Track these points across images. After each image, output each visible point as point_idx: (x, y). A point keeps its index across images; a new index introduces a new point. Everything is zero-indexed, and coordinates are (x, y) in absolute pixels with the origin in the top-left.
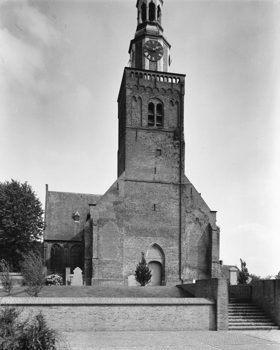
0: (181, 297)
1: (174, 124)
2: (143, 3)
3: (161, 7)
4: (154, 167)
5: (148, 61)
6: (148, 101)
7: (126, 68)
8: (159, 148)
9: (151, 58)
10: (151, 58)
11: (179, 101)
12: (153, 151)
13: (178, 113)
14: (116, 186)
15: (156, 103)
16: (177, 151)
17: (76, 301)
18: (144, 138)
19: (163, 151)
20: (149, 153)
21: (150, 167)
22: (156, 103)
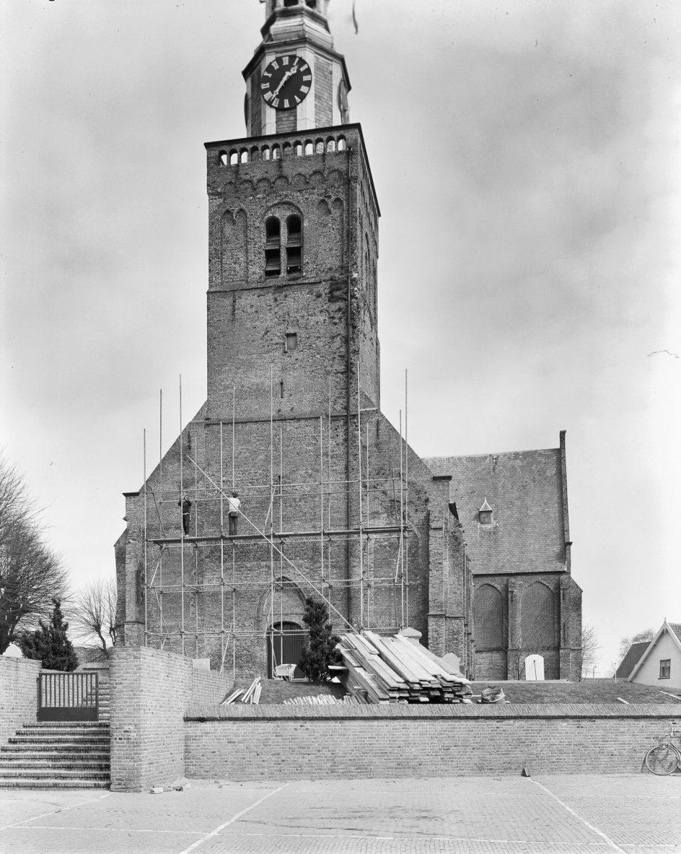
1: (332, 261)
4: (278, 380)
5: (273, 112)
8: (291, 330)
10: (281, 103)
11: (342, 197)
15: (282, 215)
16: (340, 329)
18: (254, 310)
19: (302, 334)
20: (266, 348)
22: (282, 215)
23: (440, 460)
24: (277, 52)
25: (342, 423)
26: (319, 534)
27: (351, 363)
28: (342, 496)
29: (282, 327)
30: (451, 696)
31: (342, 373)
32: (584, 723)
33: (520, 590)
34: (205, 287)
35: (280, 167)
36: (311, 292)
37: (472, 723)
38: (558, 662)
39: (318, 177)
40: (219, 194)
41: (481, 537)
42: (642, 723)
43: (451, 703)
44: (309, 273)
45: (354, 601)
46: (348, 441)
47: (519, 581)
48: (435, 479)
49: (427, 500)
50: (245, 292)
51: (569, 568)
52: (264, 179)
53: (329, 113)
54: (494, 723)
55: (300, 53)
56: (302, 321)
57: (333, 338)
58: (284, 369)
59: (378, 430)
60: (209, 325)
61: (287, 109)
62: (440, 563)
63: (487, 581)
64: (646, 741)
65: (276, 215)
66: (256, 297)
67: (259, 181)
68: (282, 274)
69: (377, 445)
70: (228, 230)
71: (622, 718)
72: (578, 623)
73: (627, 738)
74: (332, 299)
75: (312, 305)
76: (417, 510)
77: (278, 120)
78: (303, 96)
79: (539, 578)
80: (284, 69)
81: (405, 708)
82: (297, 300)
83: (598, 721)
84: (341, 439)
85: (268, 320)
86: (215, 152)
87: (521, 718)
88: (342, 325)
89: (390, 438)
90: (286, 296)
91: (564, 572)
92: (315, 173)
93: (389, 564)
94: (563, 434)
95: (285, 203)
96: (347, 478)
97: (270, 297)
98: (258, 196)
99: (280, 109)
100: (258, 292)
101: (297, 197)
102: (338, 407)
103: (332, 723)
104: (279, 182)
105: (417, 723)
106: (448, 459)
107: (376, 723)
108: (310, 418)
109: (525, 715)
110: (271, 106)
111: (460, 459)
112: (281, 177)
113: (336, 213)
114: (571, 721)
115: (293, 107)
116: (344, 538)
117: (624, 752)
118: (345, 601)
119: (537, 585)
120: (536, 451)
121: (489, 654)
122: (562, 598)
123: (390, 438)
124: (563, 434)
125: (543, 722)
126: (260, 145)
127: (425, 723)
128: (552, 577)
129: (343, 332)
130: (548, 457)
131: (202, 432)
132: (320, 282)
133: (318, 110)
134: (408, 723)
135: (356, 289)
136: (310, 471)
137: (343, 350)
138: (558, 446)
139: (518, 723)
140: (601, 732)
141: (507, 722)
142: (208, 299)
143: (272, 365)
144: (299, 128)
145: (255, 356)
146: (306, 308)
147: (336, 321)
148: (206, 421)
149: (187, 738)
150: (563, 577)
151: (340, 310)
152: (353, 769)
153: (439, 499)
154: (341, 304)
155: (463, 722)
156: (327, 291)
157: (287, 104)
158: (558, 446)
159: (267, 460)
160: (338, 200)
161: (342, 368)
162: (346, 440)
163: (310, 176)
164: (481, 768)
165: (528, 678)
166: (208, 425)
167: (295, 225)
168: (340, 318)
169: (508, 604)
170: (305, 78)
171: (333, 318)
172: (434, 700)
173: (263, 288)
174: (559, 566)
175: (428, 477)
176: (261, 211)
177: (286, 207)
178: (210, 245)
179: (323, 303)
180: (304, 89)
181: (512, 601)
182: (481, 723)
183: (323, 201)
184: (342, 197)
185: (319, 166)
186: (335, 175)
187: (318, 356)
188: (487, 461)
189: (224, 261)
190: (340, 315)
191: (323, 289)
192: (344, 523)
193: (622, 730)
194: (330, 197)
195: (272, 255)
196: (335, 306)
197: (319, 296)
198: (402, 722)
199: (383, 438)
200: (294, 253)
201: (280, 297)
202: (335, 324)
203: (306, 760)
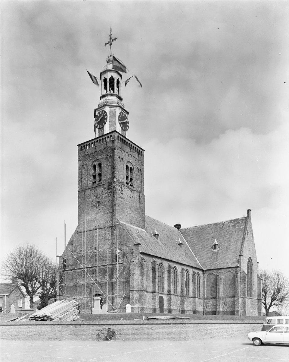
0: (212, 315)
1: (109, 176)
2: (105, 77)
3: (120, 80)
4: (95, 217)
5: (98, 129)
6: (92, 164)
7: (82, 147)
8: (98, 201)
9: (100, 126)
10: (100, 126)
11: (111, 155)
12: (95, 204)
13: (218, 292)
14: (72, 239)
15: (96, 163)
16: (111, 198)
17: (200, 321)
18: (89, 195)
19: (101, 201)
20: (92, 207)
21: (92, 218)
22: (96, 163)
23: (204, 226)
24: (99, 111)
25: (111, 229)
26: (97, 266)
27: (113, 209)
28: (111, 252)
29: (96, 200)
30: (46, 319)
31: (111, 212)
32: (77, 326)
33: (222, 275)
34: (78, 190)
35: (96, 148)
36: (103, 188)
37: (46, 326)
38: (235, 302)
39: (105, 150)
40: (81, 160)
41: (212, 255)
42: (95, 326)
43: (46, 321)
44: (103, 182)
45: (114, 286)
46: (112, 235)
47: (221, 272)
48: (135, 245)
49: (133, 252)
50: (87, 190)
51: (240, 265)
52: (92, 153)
53: (115, 125)
54: (52, 326)
55: (104, 110)
56: (101, 197)
57: (109, 201)
58: (97, 213)
59: (120, 230)
60: (78, 202)
61: (102, 128)
62: (133, 273)
63: (211, 272)
64: (96, 331)
65: (95, 164)
66: (89, 191)
67: (90, 154)
68: (97, 182)
69: (120, 235)
70: (83, 171)
71: (89, 325)
72: (244, 286)
73: (90, 330)
74: (109, 189)
75: (104, 191)
76: (130, 256)
77: (99, 132)
78: (105, 123)
79: (229, 270)
80: (100, 115)
81: (34, 322)
82: (101, 189)
83: (82, 326)
84: (110, 234)
85: (92, 198)
86: (80, 147)
87: (28, 325)
88: (111, 197)
89: (123, 232)
90: (97, 190)
91: (238, 267)
92: (104, 149)
93: (123, 274)
94: (249, 211)
95: (97, 160)
96: (112, 247)
97: (93, 190)
98: (91, 159)
99: (99, 128)
100: (90, 189)
101: (100, 157)
102: (110, 224)
103: (11, 326)
104: (95, 153)
105: (32, 326)
106: (207, 225)
107: (22, 326)
108: (103, 228)
109: (60, 324)
110: (97, 128)
111: (211, 225)
112: (96, 152)
113: (110, 160)
114: (74, 326)
115: (103, 127)
116: (111, 266)
117: (89, 334)
118: (111, 286)
119: (229, 272)
120: (239, 219)
121: (212, 300)
122: (236, 277)
123: (123, 232)
124: (249, 211)
125: (66, 326)
126: (104, 137)
127: (34, 326)
128: (234, 269)
129: (111, 199)
130: (243, 220)
131: (76, 235)
132: (105, 184)
133: (110, 126)
134: (30, 326)
135: (115, 184)
136: (103, 245)
137: (111, 205)
138: (246, 216)
139: (58, 326)
140: (82, 329)
141: (55, 326)
142: (78, 193)
143: (94, 212)
144: (104, 134)
145: (89, 210)
146: (102, 192)
147: (109, 196)
148: (78, 232)
149: (284, 332)
150: (238, 269)
151: (110, 192)
152: (16, 338)
153: (136, 251)
154: (111, 190)
155: (44, 326)
156: (107, 186)
157: (101, 127)
158: (246, 216)
159: (92, 243)
160: (110, 156)
161: (111, 211)
162: (112, 234)
163: (103, 150)
164: (48, 338)
165: (127, 312)
166: (78, 233)
167: (100, 165)
168: (110, 195)
169: (217, 280)
170: (106, 117)
171: (109, 195)
172: (43, 320)
173: (91, 188)
174: (236, 265)
175: (133, 244)
176: (91, 163)
177: (97, 161)
178: (79, 176)
179: (106, 191)
180: (105, 121)
181: (218, 279)
182: (49, 326)
183: (106, 157)
184: (111, 155)
185: (105, 146)
186: (109, 148)
187: (105, 208)
188: (220, 224)
189: (82, 181)
190: (110, 194)
191: (106, 186)
192: (111, 261)
193: (89, 328)
194: (108, 156)
195: (94, 177)
196: (109, 191)
197: (105, 188)
198: (28, 326)
199: (122, 232)
200: (100, 175)
201: (95, 190)
202: (109, 197)
203: (5, 335)
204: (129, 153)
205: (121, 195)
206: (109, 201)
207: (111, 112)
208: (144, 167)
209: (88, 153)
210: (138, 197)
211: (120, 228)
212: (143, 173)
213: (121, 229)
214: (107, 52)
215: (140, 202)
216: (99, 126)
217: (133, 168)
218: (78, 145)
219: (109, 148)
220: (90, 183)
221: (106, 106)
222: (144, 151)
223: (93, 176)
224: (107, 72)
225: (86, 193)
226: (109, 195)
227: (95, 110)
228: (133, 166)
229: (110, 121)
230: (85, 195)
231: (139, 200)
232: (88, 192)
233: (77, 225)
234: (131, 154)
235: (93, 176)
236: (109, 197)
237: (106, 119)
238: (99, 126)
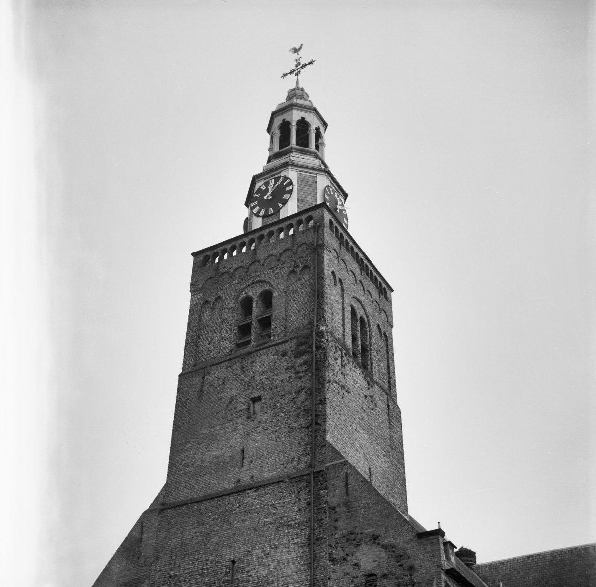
3: (322, 130)
6: (239, 296)
15: (254, 293)
16: (306, 382)
18: (221, 381)
21: (228, 453)
22: (254, 293)
24: (265, 179)
40: (200, 290)
61: (272, 214)
65: (250, 294)
66: (224, 370)
68: (252, 344)
74: (297, 355)
90: (253, 362)
95: (258, 282)
102: (302, 466)
131: (155, 520)
136: (267, 549)
145: (217, 428)
151: (305, 363)
168: (306, 371)
170: (286, 197)
173: (230, 360)
204: (359, 277)
205: (340, 376)
206: (300, 391)
207: (301, 180)
208: (394, 329)
209: (226, 269)
210: (386, 407)
211: (347, 476)
212: (392, 344)
213: (350, 481)
214: (290, 83)
215: (390, 423)
216: (258, 208)
217: (368, 320)
218: (194, 255)
219: (301, 249)
220: (227, 345)
221: (290, 167)
222: (392, 291)
223: (239, 327)
224: (292, 109)
225: (209, 378)
226: (299, 372)
227: (255, 179)
228: (367, 315)
229: (298, 200)
230: (206, 381)
231: (386, 415)
232: (216, 375)
233: (163, 481)
234: (363, 281)
235: (239, 327)
236: (301, 378)
237: (290, 192)
238: (258, 208)
